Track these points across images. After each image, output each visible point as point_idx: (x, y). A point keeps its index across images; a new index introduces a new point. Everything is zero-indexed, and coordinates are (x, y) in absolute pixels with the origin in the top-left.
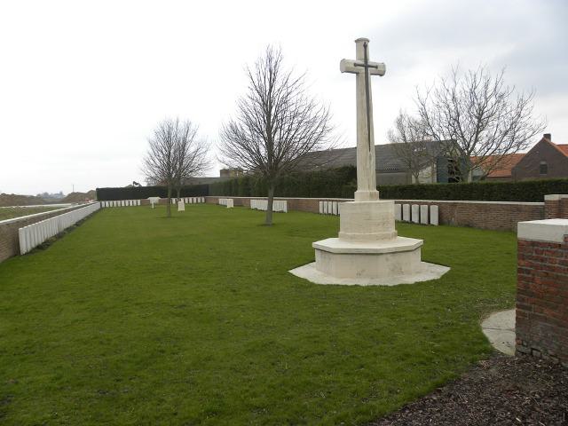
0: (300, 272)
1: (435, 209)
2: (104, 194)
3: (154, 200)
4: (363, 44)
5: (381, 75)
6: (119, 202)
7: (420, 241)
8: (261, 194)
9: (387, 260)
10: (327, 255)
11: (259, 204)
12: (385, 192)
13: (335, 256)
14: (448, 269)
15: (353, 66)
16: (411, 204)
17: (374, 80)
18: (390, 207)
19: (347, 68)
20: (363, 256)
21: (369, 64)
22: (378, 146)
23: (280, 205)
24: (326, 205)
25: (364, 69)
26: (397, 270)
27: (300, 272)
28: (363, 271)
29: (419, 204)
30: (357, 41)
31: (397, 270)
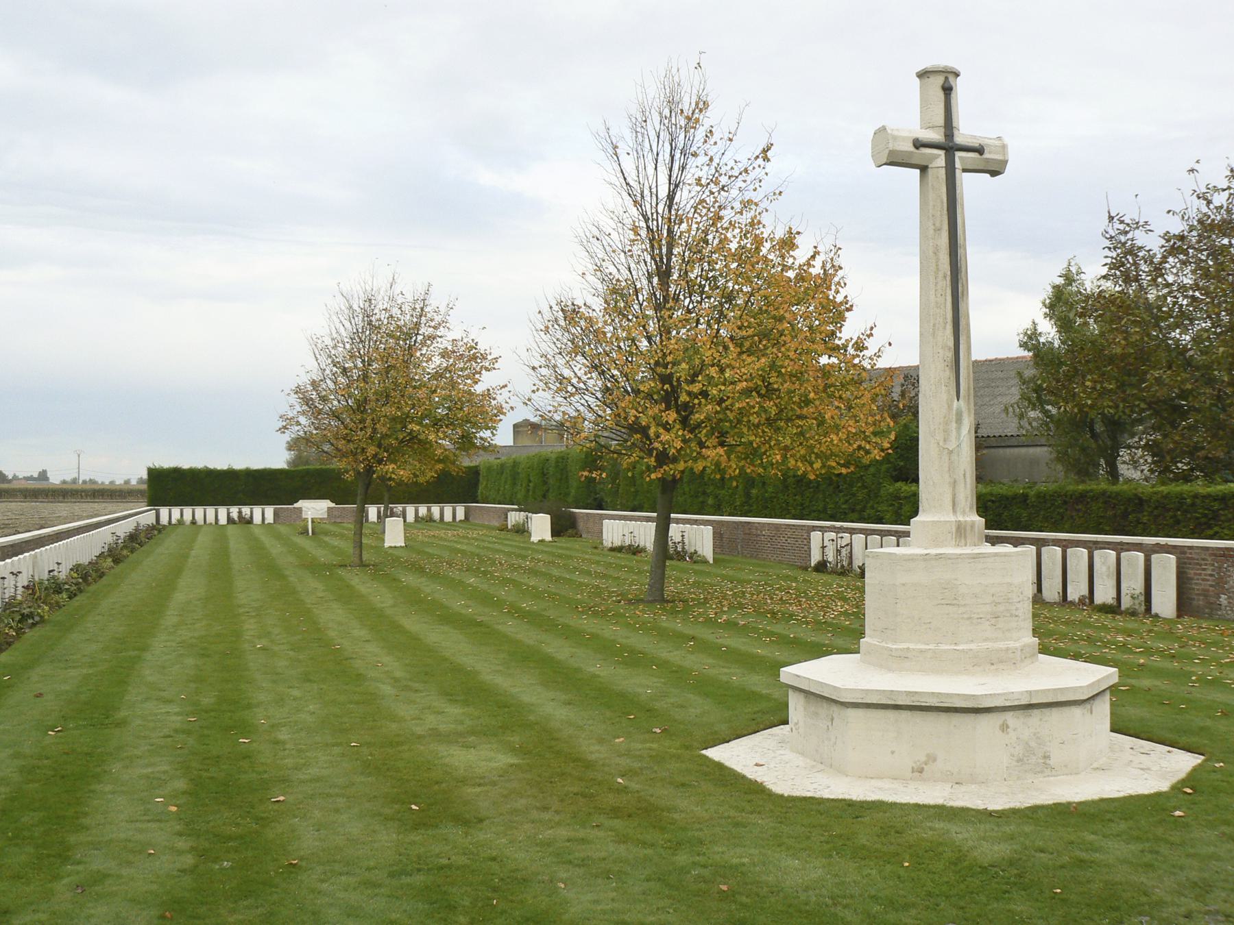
0: (736, 755)
1: (1166, 569)
2: (168, 486)
3: (314, 509)
4: (943, 82)
5: (994, 173)
6: (211, 511)
7: (1104, 674)
8: (631, 499)
9: (1004, 727)
10: (824, 710)
11: (624, 529)
12: (1004, 511)
13: (851, 712)
14: (1183, 763)
15: (912, 149)
16: (1092, 547)
17: (971, 185)
18: (1012, 565)
19: (891, 153)
20: (944, 716)
21: (959, 139)
22: (976, 361)
23: (696, 535)
24: (823, 540)
25: (945, 157)
26: (1039, 762)
27: (736, 755)
28: (932, 759)
29: (1119, 548)
30: (923, 75)
31: (1039, 762)
